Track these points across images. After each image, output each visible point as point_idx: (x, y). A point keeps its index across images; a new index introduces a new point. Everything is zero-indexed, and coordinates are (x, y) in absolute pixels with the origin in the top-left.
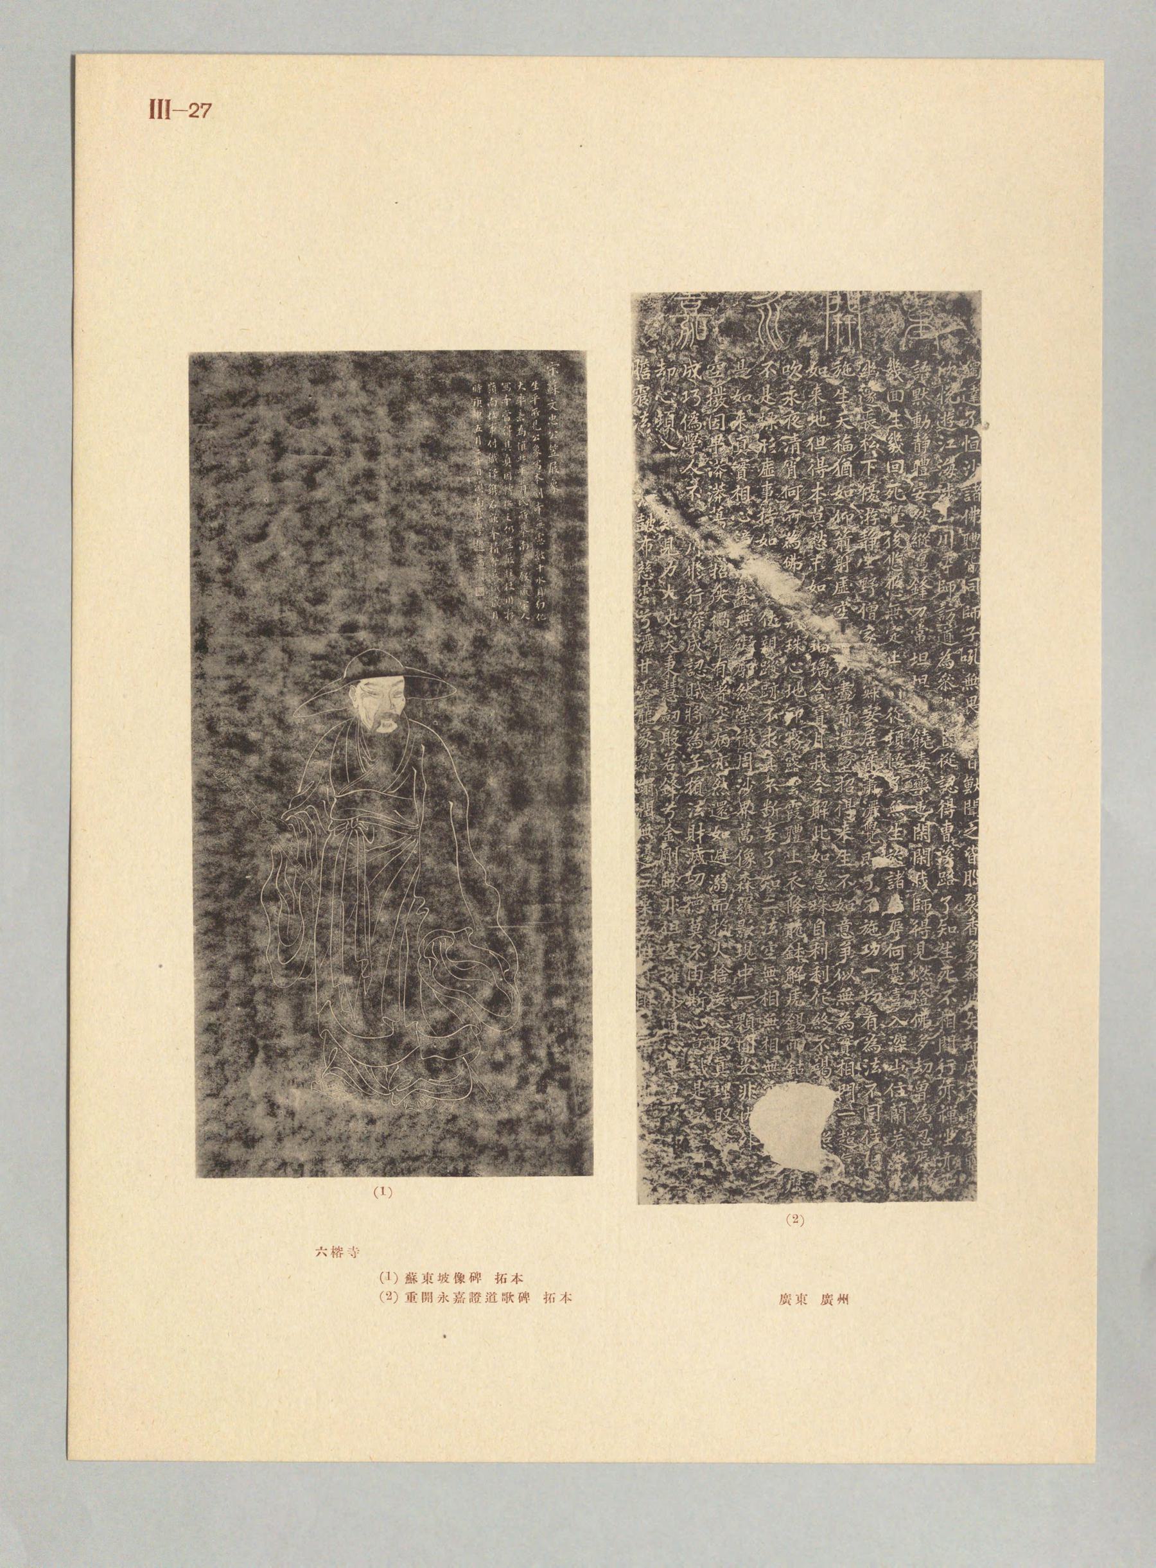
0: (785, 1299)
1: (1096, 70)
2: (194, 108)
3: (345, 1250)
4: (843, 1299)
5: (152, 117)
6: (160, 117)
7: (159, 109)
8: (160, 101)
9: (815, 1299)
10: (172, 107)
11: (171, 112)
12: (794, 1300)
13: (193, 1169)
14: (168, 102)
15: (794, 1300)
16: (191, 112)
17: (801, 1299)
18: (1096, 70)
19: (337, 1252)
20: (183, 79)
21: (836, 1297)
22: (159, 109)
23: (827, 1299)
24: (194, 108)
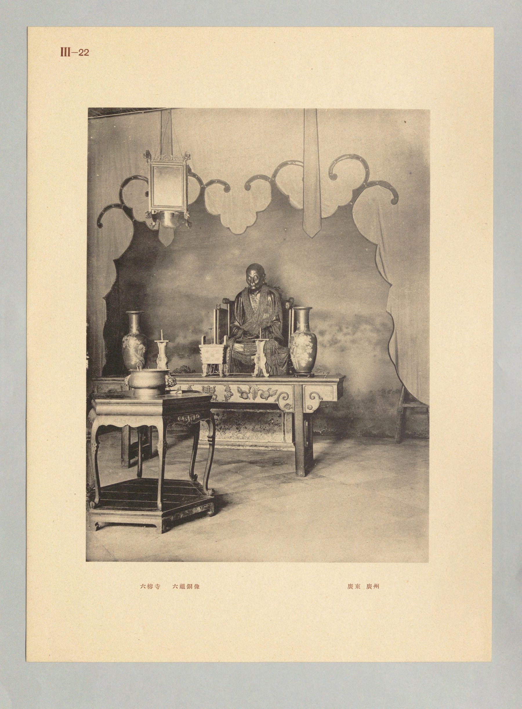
0: (350, 586)
2: (81, 51)
3: (154, 586)
4: (376, 586)
5: (62, 55)
6: (66, 48)
7: (65, 52)
8: (66, 48)
9: (364, 586)
10: (71, 52)
12: (354, 587)
14: (69, 48)
15: (354, 587)
18: (487, 34)
19: (150, 586)
20: (74, 37)
21: (373, 585)
22: (65, 52)
23: (369, 586)
24: (81, 51)
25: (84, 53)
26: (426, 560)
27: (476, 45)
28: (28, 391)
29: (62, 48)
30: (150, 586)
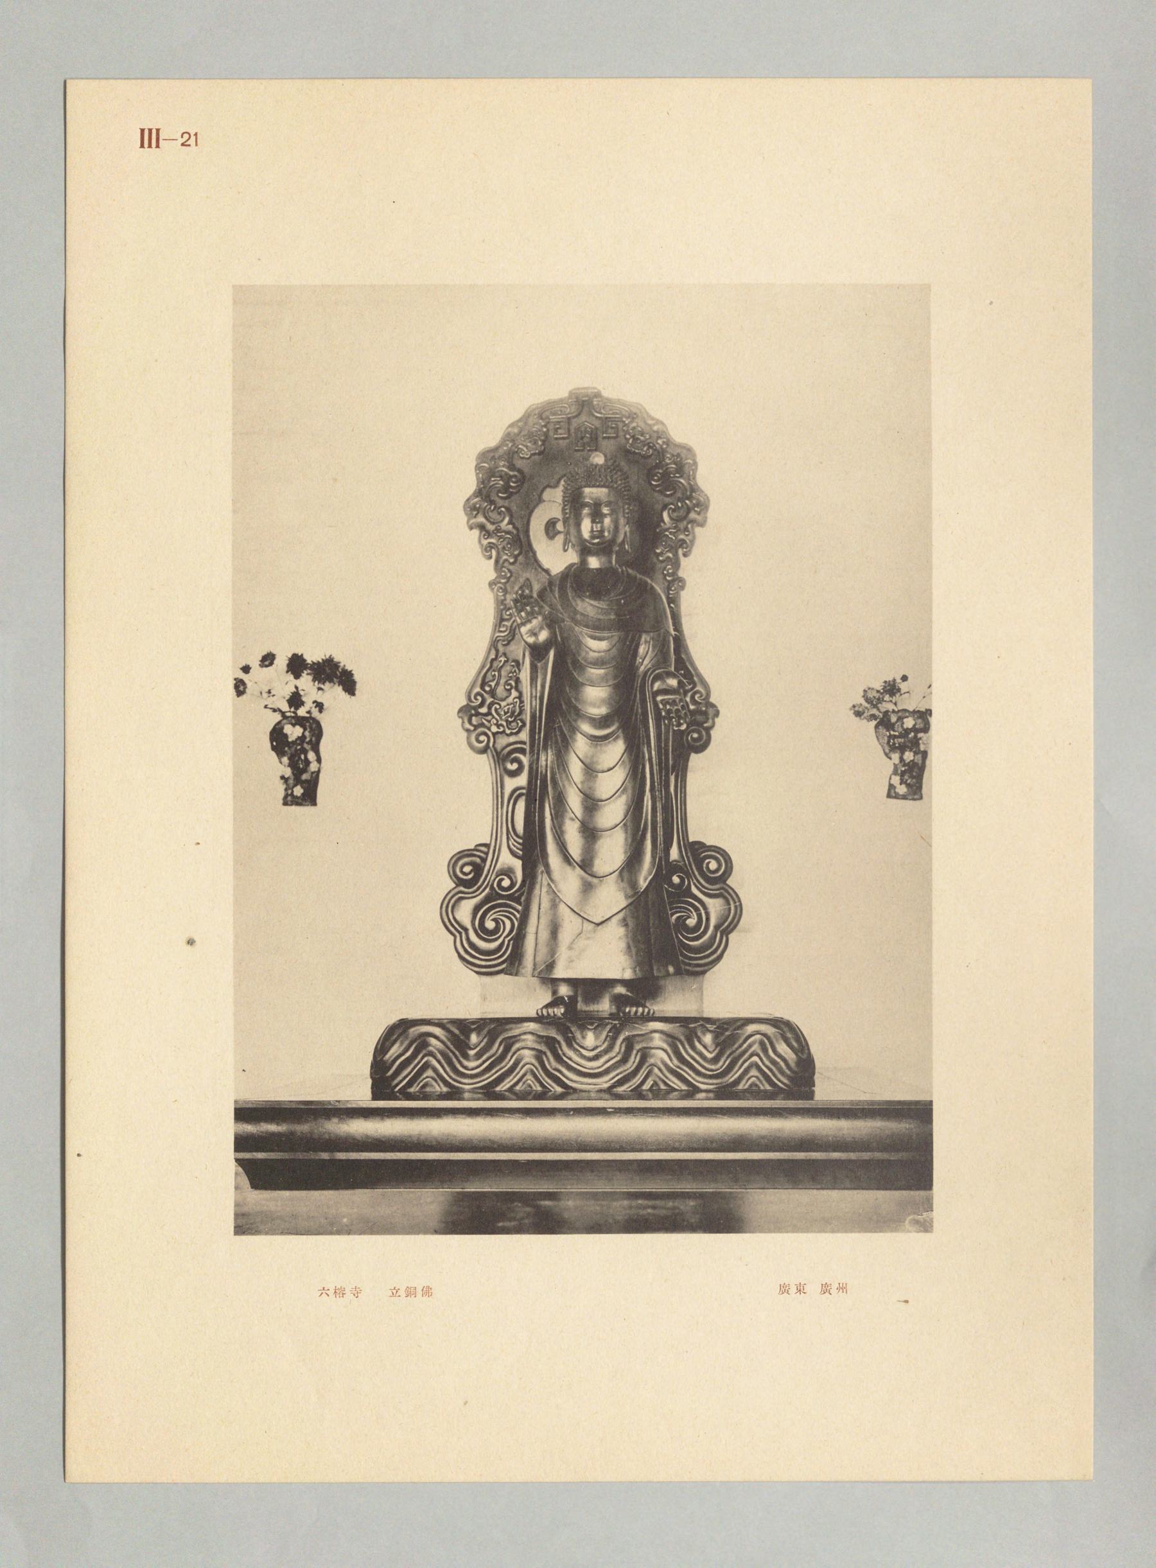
1: (1081, 90)
2: (186, 136)
3: (347, 1291)
4: (842, 1288)
5: (142, 146)
6: (150, 130)
7: (150, 138)
8: (150, 130)
9: (813, 1289)
11: (161, 141)
12: (402, 1293)
13: (902, 1244)
14: (158, 130)
15: (793, 1290)
16: (181, 141)
17: (800, 1290)
18: (1081, 90)
19: (339, 1292)
20: (167, 102)
22: (150, 138)
23: (826, 1289)
24: (186, 136)
25: (188, 139)
26: (926, 1227)
27: (1048, 124)
28: (68, 599)
29: (142, 131)
30: (339, 1292)
